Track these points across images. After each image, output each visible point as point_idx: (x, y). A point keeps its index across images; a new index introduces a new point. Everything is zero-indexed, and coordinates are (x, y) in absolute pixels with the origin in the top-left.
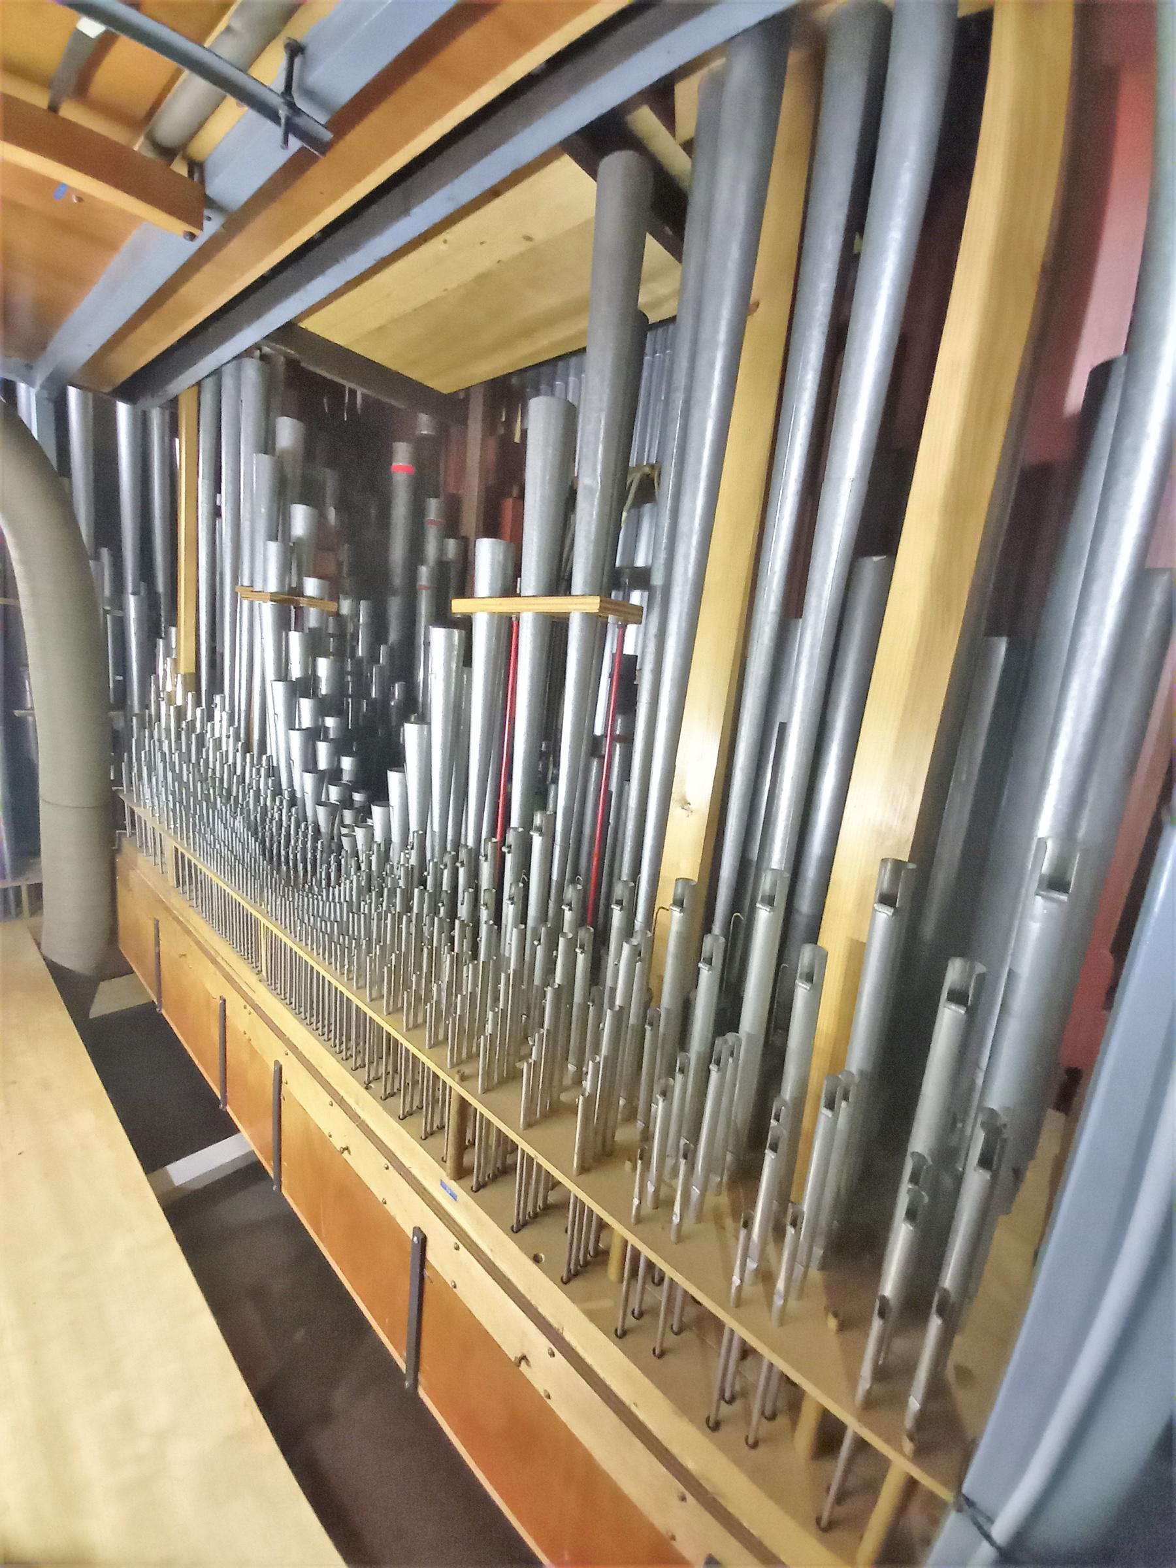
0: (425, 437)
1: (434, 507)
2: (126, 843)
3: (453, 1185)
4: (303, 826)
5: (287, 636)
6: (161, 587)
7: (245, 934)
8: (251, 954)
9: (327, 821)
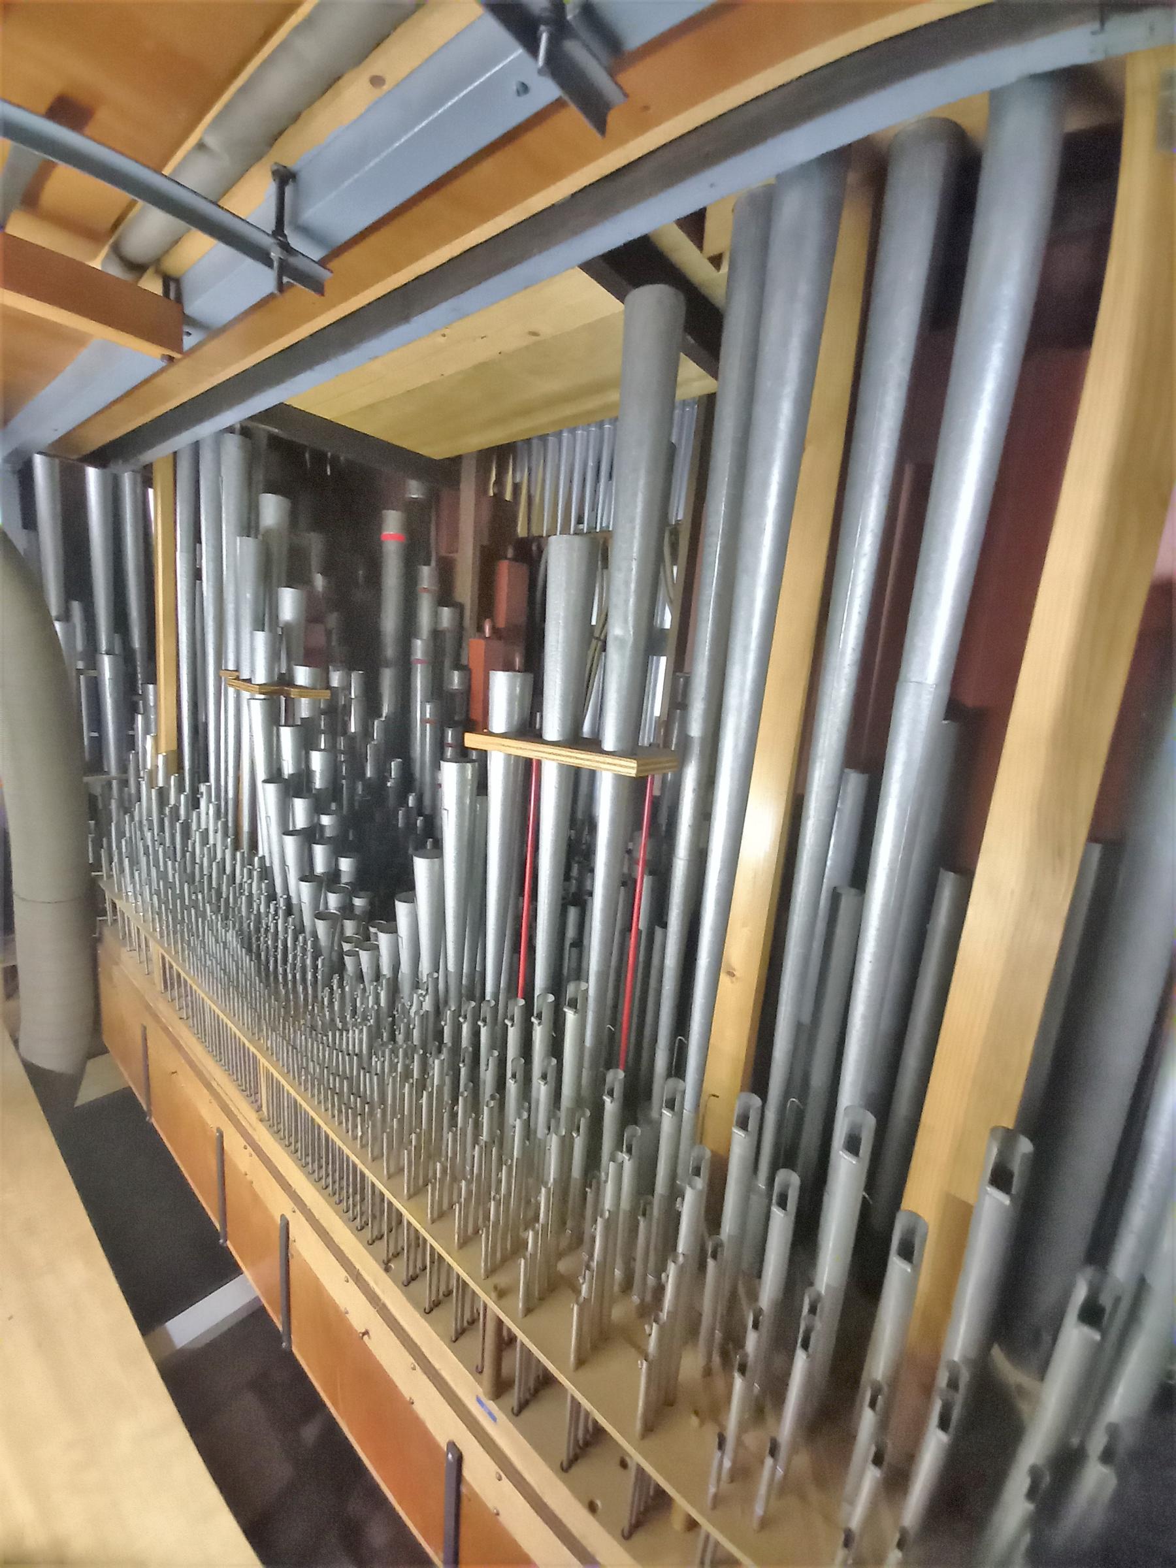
0: (415, 501)
1: (427, 575)
2: (107, 932)
3: (492, 1405)
4: (301, 938)
5: (278, 730)
6: (137, 644)
7: (246, 1074)
8: (251, 1092)
9: (328, 934)
